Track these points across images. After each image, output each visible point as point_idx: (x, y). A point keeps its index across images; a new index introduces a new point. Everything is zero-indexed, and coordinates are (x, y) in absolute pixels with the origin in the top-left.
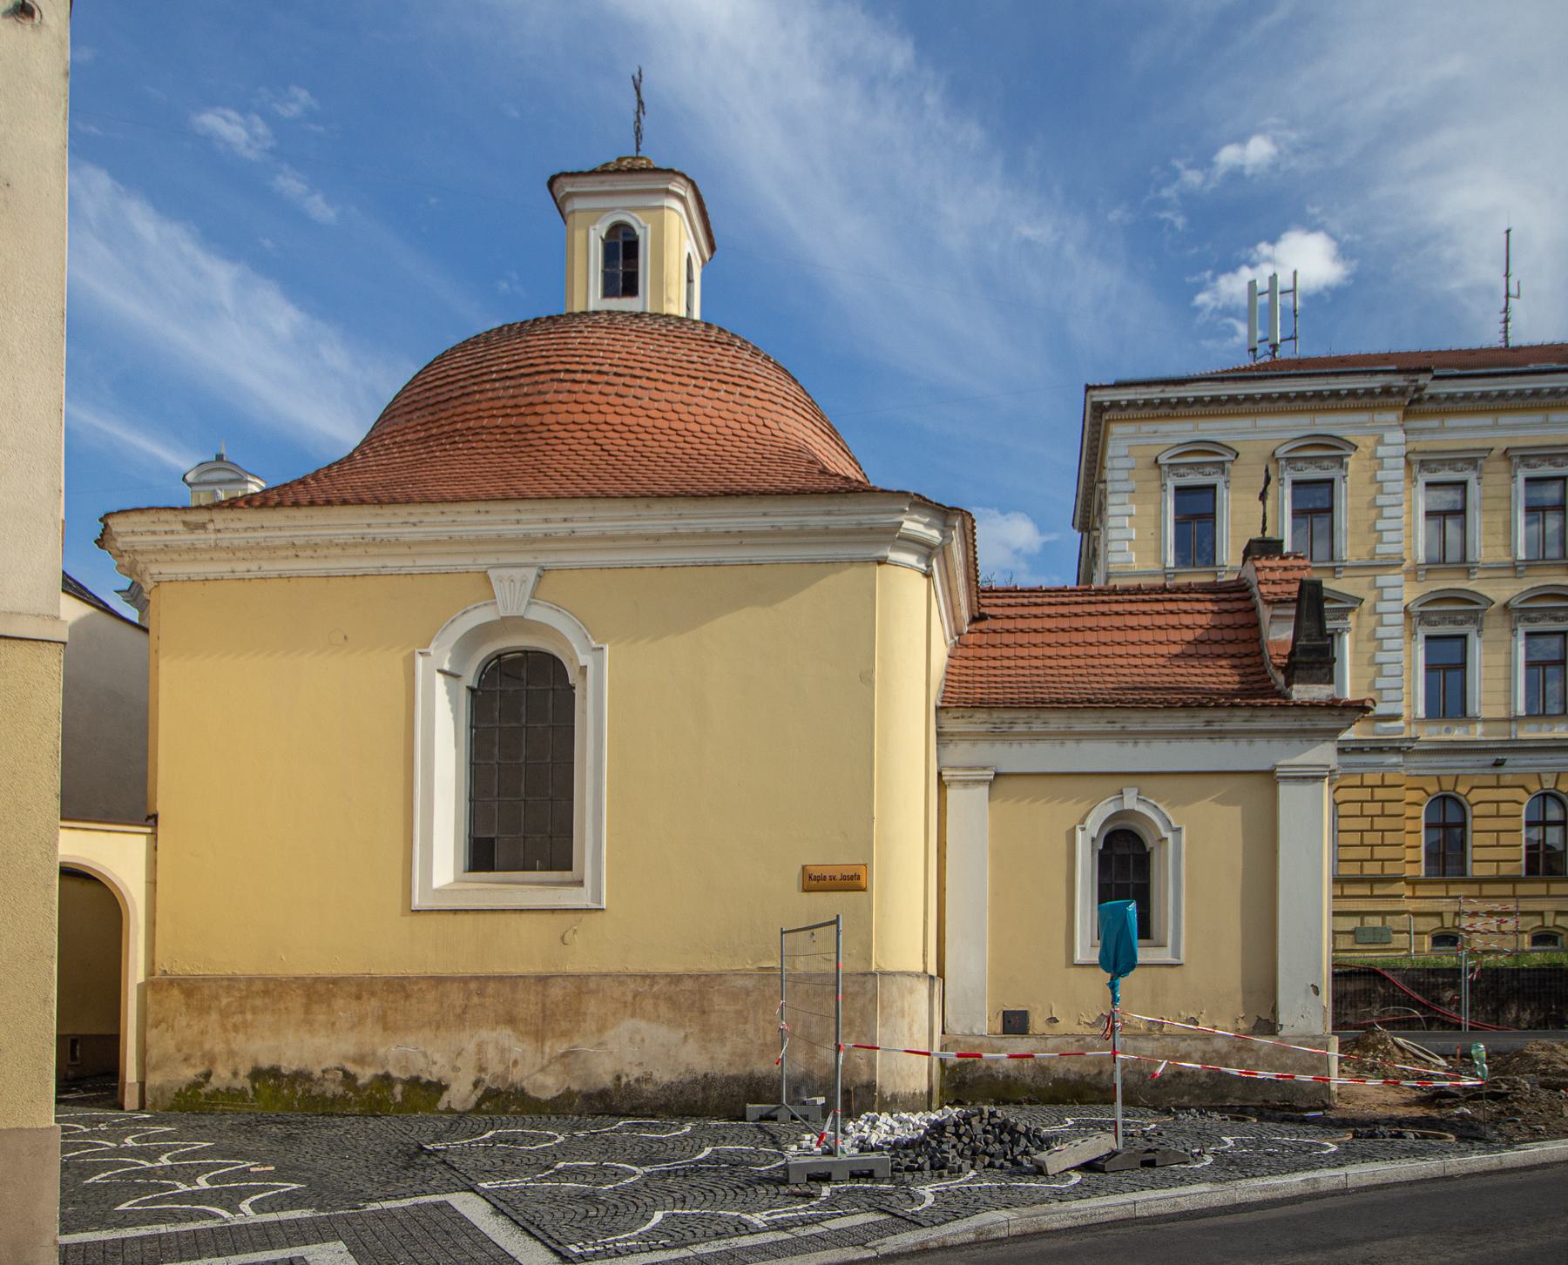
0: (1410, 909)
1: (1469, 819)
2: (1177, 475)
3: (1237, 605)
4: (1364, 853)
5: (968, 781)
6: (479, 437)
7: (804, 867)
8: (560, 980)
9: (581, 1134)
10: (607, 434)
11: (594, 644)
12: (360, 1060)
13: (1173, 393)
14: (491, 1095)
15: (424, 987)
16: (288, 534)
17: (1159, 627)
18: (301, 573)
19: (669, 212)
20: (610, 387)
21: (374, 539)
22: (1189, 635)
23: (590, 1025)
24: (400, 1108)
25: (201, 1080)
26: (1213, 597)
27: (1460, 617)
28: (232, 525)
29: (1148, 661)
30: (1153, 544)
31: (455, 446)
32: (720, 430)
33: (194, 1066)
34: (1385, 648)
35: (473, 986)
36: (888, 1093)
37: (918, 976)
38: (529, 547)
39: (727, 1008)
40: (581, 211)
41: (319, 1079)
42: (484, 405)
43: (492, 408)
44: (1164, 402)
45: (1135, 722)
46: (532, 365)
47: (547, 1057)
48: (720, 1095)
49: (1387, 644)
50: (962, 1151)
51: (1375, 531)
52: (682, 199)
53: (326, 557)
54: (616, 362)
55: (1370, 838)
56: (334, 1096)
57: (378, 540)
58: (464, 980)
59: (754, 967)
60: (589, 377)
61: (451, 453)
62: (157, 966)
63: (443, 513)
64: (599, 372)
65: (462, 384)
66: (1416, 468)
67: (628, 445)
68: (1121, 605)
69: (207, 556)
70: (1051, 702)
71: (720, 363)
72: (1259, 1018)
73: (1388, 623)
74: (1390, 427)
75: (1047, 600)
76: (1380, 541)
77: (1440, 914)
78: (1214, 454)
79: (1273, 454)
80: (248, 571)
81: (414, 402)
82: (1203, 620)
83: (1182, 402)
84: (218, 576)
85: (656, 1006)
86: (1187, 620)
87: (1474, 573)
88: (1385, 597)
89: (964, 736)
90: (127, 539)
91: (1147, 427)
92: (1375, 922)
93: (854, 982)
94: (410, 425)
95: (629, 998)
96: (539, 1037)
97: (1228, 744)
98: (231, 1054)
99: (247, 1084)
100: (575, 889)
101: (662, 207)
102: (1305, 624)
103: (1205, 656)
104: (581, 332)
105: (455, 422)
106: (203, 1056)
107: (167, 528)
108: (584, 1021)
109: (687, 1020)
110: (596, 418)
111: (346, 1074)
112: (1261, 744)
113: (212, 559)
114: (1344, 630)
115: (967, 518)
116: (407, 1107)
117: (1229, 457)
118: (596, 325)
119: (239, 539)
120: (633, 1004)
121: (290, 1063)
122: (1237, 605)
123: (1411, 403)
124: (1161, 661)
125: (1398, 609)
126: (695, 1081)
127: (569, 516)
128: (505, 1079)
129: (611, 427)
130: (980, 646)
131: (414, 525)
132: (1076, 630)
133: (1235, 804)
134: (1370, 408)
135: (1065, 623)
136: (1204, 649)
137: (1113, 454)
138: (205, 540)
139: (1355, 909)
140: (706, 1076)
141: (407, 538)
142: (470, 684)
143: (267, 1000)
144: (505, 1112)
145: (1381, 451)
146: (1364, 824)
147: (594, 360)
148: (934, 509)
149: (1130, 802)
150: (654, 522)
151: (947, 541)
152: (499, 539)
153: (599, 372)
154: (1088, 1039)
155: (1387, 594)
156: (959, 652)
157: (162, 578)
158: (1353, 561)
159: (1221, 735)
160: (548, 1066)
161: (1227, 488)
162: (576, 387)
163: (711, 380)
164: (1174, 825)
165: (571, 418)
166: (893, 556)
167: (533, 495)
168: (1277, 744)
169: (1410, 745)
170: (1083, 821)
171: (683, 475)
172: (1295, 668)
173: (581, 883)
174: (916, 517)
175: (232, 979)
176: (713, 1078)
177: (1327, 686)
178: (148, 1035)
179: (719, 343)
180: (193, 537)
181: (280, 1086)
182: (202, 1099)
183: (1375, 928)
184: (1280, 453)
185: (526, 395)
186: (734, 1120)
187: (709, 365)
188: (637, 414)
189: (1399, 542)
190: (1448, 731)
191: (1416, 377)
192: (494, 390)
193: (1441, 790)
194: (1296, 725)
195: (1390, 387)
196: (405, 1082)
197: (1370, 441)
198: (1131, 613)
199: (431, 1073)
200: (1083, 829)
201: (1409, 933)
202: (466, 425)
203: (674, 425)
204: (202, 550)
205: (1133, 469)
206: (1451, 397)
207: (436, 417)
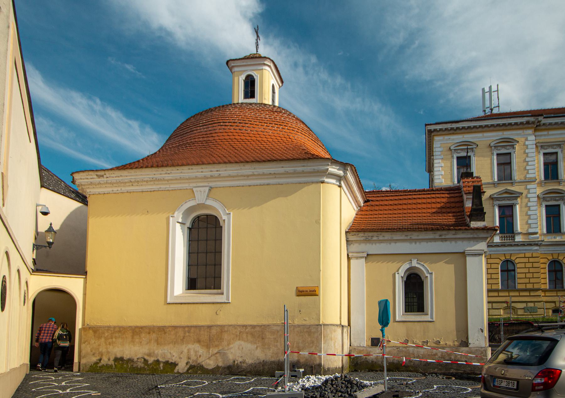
0: (544, 300)
1: (516, 269)
2: (457, 153)
3: (456, 195)
4: (527, 281)
5: (358, 257)
6: (194, 145)
7: (297, 287)
8: (215, 327)
9: (214, 382)
10: (235, 143)
11: (227, 212)
12: (149, 355)
13: (454, 126)
14: (192, 367)
15: (170, 330)
16: (129, 178)
17: (429, 203)
18: (134, 191)
19: (265, 71)
20: (237, 127)
21: (156, 179)
22: (439, 206)
23: (225, 343)
24: (162, 372)
25: (98, 361)
26: (448, 192)
27: (557, 199)
28: (112, 175)
29: (424, 215)
30: (450, 176)
31: (186, 148)
32: (273, 140)
33: (96, 357)
34: (531, 209)
35: (186, 329)
36: (326, 367)
37: (337, 325)
38: (206, 180)
39: (271, 337)
40: (237, 71)
41: (136, 361)
42: (197, 134)
43: (199, 135)
44: (452, 129)
45: (415, 235)
46: (213, 121)
47: (210, 354)
48: (268, 368)
49: (532, 208)
50: (333, 390)
51: (526, 170)
52: (269, 66)
53: (142, 185)
54: (240, 119)
55: (528, 275)
56: (141, 367)
57: (157, 179)
58: (184, 327)
59: (280, 323)
60: (231, 124)
61: (190, 150)
62: (86, 322)
63: (178, 170)
64: (234, 122)
65: (191, 128)
66: (539, 148)
67: (242, 146)
68: (411, 196)
69: (104, 186)
70: (386, 229)
71: (276, 118)
72: (462, 341)
73: (532, 201)
74: (529, 135)
75: (400, 194)
76: (528, 173)
77: (555, 302)
78: (469, 146)
79: (490, 145)
80: (118, 190)
81: (177, 134)
82: (444, 200)
83: (458, 128)
84: (108, 192)
85: (247, 336)
86: (438, 200)
87: (562, 183)
88: (530, 192)
89: (356, 241)
90: (79, 181)
91: (447, 137)
92: (532, 305)
93: (314, 328)
94: (174, 141)
95: (238, 334)
96: (208, 347)
97: (448, 243)
98: (108, 352)
99: (113, 363)
100: (221, 296)
101: (263, 69)
102: (475, 200)
103: (444, 213)
104: (230, 110)
105: (187, 140)
106: (99, 353)
107: (91, 177)
108: (223, 341)
109: (257, 341)
110: (232, 137)
111: (145, 359)
112: (460, 243)
113: (106, 187)
114: (516, 204)
115: (352, 167)
116: (164, 371)
117: (474, 146)
118: (236, 107)
119: (114, 180)
120: (239, 336)
121: (127, 356)
122: (456, 195)
123: (537, 126)
124: (429, 215)
125: (535, 196)
126: (260, 363)
127: (218, 169)
128: (196, 362)
129: (236, 140)
130: (367, 211)
131: (169, 174)
132: (400, 204)
133: (452, 264)
134: (522, 128)
135: (396, 202)
136: (444, 210)
137: (436, 146)
138: (103, 180)
139: (524, 300)
140: (264, 361)
141: (166, 178)
142: (188, 227)
143: (120, 334)
144: (196, 373)
145: (527, 143)
146: (526, 270)
147: (233, 118)
148: (340, 164)
149: (415, 263)
150: (246, 171)
151: (346, 175)
152: (196, 178)
153: (234, 122)
154: (401, 348)
155: (531, 191)
156: (360, 213)
157: (91, 193)
158: (519, 180)
159: (446, 240)
160: (211, 357)
161: (474, 157)
162: (226, 127)
163: (272, 124)
164: (430, 272)
165: (223, 137)
166: (326, 180)
167: (206, 163)
168: (465, 243)
169: (541, 243)
170: (398, 271)
171: (258, 155)
172: (472, 216)
173: (222, 294)
174: (334, 167)
175: (109, 327)
176: (266, 362)
177: (483, 222)
178: (82, 346)
179: (276, 112)
180: (100, 180)
181: (123, 364)
182: (98, 368)
183: (531, 307)
184: (492, 144)
185: (210, 130)
186: (271, 377)
187: (272, 119)
188: (245, 135)
189: (535, 173)
190: (555, 238)
191: (538, 118)
192: (200, 129)
193: (553, 258)
194: (471, 236)
195: (529, 121)
196: (164, 363)
197: (523, 139)
198: (419, 198)
199: (172, 360)
200: (398, 273)
201: (544, 309)
202: (190, 141)
203: (258, 139)
204: (103, 184)
205: (442, 151)
206: (550, 124)
207: (182, 139)
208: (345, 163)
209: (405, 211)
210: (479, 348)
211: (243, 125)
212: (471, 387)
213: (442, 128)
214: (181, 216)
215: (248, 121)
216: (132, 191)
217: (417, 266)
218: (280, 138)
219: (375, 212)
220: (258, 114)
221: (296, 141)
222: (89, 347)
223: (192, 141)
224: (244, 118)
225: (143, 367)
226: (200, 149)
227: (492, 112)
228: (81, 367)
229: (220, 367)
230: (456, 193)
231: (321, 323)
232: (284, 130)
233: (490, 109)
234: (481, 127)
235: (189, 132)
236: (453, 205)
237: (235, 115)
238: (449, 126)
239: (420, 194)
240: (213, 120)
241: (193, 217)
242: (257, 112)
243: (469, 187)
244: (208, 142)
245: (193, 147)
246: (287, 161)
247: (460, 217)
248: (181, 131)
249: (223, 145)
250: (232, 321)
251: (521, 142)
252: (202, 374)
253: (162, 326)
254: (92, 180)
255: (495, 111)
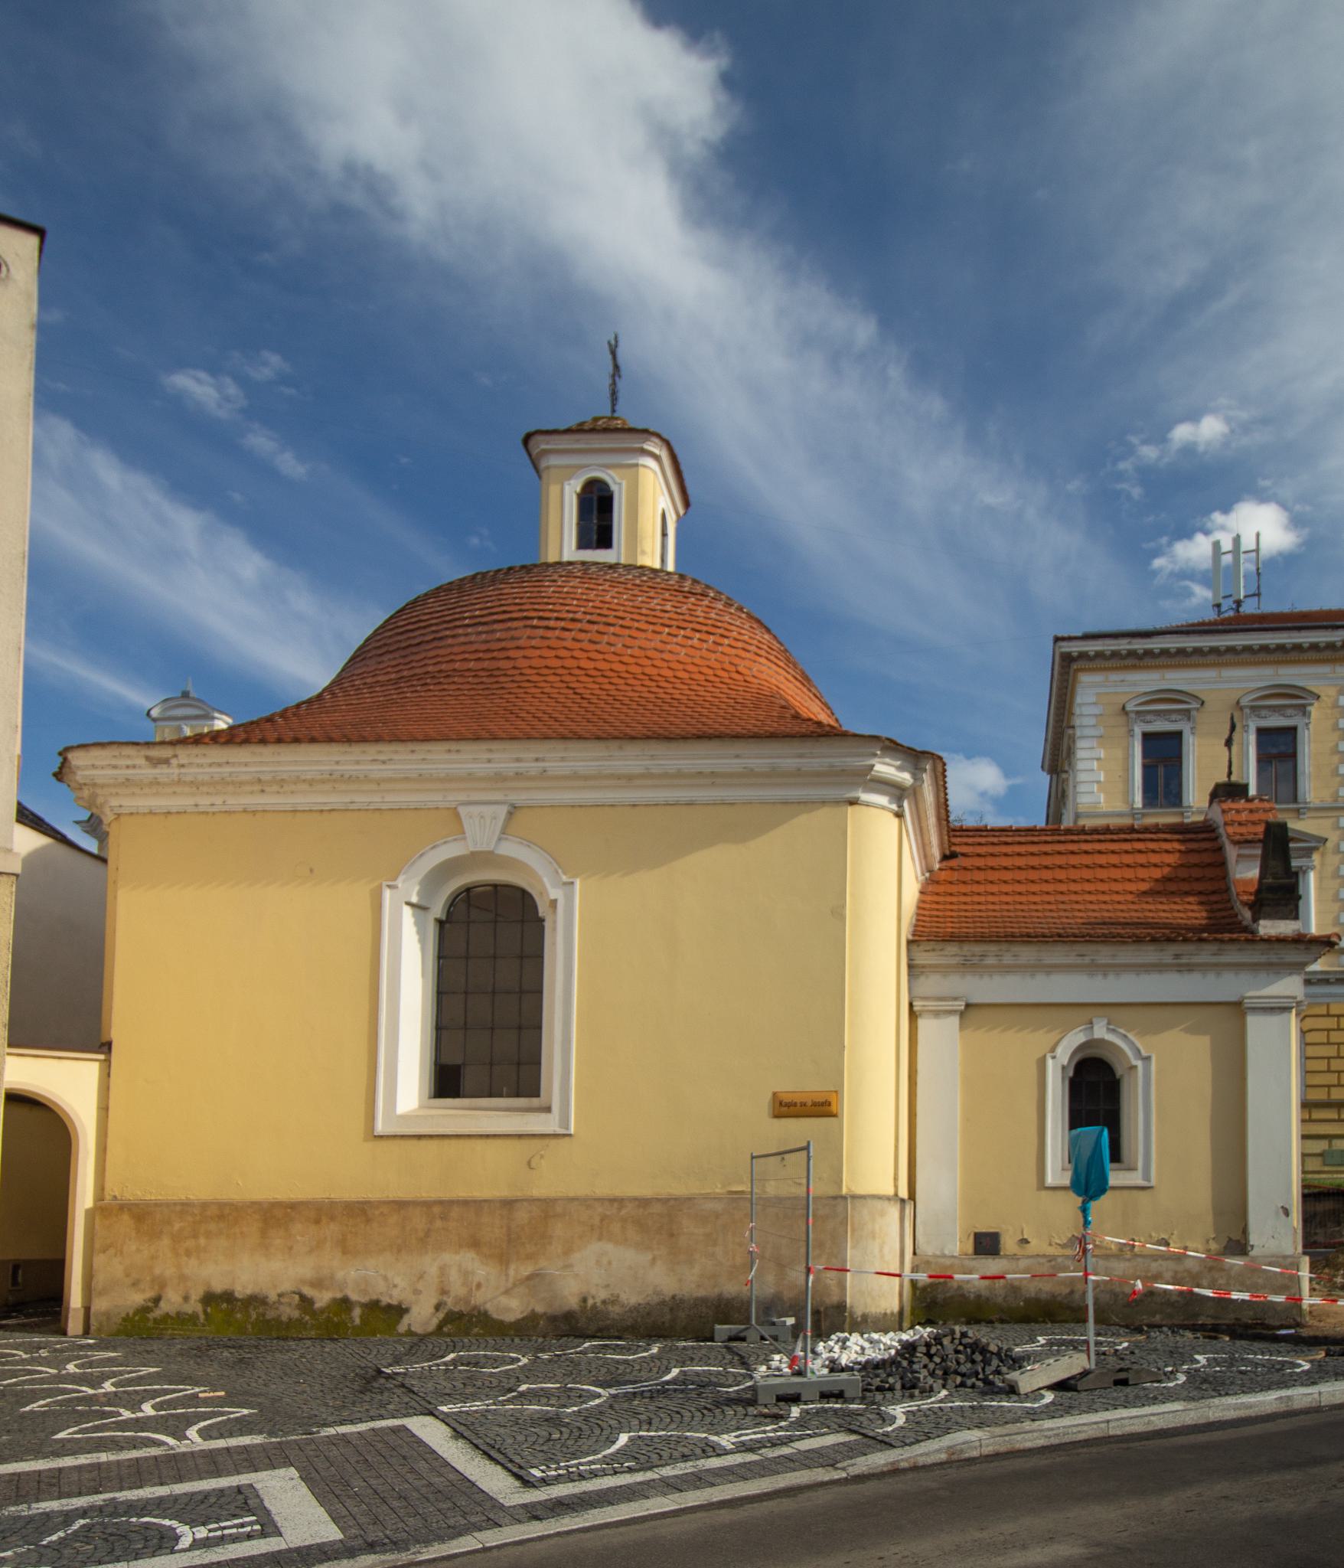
5: (939, 1011)
6: (451, 680)
7: (774, 1094)
8: (525, 1203)
11: (565, 878)
12: (318, 1283)
13: (1139, 645)
14: (452, 1318)
18: (267, 808)
20: (583, 634)
21: (342, 776)
22: (1157, 873)
25: (150, 1304)
33: (143, 1291)
35: (436, 1210)
36: (858, 1312)
37: (888, 1198)
40: (555, 467)
41: (274, 1303)
42: (456, 650)
44: (1132, 654)
45: (1104, 954)
46: (505, 612)
47: (511, 1280)
52: (657, 458)
53: (292, 792)
57: (347, 776)
58: (427, 1205)
60: (563, 624)
61: (423, 694)
62: (108, 1191)
63: (413, 751)
64: (573, 620)
70: (1006, 936)
71: (693, 613)
82: (1171, 859)
86: (1155, 859)
89: (935, 968)
90: (87, 773)
91: (1115, 677)
94: (381, 666)
95: (596, 1221)
96: (503, 1259)
98: (183, 1278)
99: (199, 1308)
101: (637, 465)
103: (1173, 893)
106: (153, 1281)
107: (129, 762)
113: (175, 793)
115: (938, 761)
116: (366, 1329)
117: (1195, 705)
118: (570, 575)
126: (663, 1303)
128: (467, 1302)
130: (951, 883)
131: (384, 762)
136: (1172, 887)
140: (674, 1297)
142: (438, 916)
144: (467, 1334)
147: (567, 608)
149: (1100, 1032)
151: (918, 783)
152: (470, 777)
153: (573, 620)
156: (930, 888)
159: (1190, 968)
160: (512, 1288)
162: (549, 634)
164: (1144, 1053)
167: (504, 735)
168: (1245, 977)
170: (1053, 1050)
171: (656, 718)
172: (1261, 905)
173: (548, 1109)
174: (887, 760)
176: (681, 1300)
177: (1293, 922)
180: (157, 771)
181: (233, 1310)
184: (1244, 702)
185: (499, 640)
186: (702, 1341)
192: (466, 635)
194: (1263, 959)
196: (364, 1306)
198: (1100, 852)
199: (391, 1297)
200: (1054, 1058)
202: (438, 668)
204: (165, 785)
205: (1101, 715)
208: (919, 749)
209: (1063, 887)
210: (1277, 1257)
211: (601, 628)
212: (1307, 1358)
213: (1104, 651)
214: (417, 888)
215: (616, 617)
216: (260, 808)
217: (1110, 1037)
218: (711, 672)
219: (976, 888)
220: (640, 599)
221: (756, 681)
222: (120, 1263)
223: (443, 667)
224: (600, 608)
225: (297, 1320)
226: (472, 693)
227: (1238, 611)
228: (93, 1322)
229: (541, 1316)
230: (1204, 840)
231: (844, 1191)
232: (720, 649)
233: (1235, 602)
234: (1214, 651)
235: (428, 642)
236: (1196, 873)
237: (573, 599)
238: (1123, 645)
239: (1100, 841)
240: (505, 608)
241: (462, 883)
242: (636, 592)
243: (1240, 824)
244: (496, 673)
245: (446, 687)
246: (753, 740)
247: (1220, 906)
248: (399, 638)
249: (543, 684)
250: (579, 1188)
251: (1325, 699)
252: (483, 1335)
253: (358, 1202)
254: (131, 771)
255: (1249, 608)
